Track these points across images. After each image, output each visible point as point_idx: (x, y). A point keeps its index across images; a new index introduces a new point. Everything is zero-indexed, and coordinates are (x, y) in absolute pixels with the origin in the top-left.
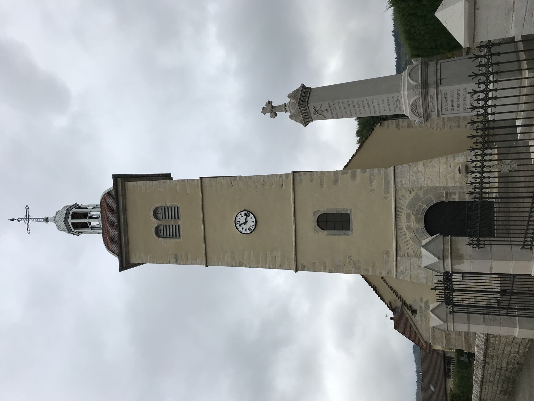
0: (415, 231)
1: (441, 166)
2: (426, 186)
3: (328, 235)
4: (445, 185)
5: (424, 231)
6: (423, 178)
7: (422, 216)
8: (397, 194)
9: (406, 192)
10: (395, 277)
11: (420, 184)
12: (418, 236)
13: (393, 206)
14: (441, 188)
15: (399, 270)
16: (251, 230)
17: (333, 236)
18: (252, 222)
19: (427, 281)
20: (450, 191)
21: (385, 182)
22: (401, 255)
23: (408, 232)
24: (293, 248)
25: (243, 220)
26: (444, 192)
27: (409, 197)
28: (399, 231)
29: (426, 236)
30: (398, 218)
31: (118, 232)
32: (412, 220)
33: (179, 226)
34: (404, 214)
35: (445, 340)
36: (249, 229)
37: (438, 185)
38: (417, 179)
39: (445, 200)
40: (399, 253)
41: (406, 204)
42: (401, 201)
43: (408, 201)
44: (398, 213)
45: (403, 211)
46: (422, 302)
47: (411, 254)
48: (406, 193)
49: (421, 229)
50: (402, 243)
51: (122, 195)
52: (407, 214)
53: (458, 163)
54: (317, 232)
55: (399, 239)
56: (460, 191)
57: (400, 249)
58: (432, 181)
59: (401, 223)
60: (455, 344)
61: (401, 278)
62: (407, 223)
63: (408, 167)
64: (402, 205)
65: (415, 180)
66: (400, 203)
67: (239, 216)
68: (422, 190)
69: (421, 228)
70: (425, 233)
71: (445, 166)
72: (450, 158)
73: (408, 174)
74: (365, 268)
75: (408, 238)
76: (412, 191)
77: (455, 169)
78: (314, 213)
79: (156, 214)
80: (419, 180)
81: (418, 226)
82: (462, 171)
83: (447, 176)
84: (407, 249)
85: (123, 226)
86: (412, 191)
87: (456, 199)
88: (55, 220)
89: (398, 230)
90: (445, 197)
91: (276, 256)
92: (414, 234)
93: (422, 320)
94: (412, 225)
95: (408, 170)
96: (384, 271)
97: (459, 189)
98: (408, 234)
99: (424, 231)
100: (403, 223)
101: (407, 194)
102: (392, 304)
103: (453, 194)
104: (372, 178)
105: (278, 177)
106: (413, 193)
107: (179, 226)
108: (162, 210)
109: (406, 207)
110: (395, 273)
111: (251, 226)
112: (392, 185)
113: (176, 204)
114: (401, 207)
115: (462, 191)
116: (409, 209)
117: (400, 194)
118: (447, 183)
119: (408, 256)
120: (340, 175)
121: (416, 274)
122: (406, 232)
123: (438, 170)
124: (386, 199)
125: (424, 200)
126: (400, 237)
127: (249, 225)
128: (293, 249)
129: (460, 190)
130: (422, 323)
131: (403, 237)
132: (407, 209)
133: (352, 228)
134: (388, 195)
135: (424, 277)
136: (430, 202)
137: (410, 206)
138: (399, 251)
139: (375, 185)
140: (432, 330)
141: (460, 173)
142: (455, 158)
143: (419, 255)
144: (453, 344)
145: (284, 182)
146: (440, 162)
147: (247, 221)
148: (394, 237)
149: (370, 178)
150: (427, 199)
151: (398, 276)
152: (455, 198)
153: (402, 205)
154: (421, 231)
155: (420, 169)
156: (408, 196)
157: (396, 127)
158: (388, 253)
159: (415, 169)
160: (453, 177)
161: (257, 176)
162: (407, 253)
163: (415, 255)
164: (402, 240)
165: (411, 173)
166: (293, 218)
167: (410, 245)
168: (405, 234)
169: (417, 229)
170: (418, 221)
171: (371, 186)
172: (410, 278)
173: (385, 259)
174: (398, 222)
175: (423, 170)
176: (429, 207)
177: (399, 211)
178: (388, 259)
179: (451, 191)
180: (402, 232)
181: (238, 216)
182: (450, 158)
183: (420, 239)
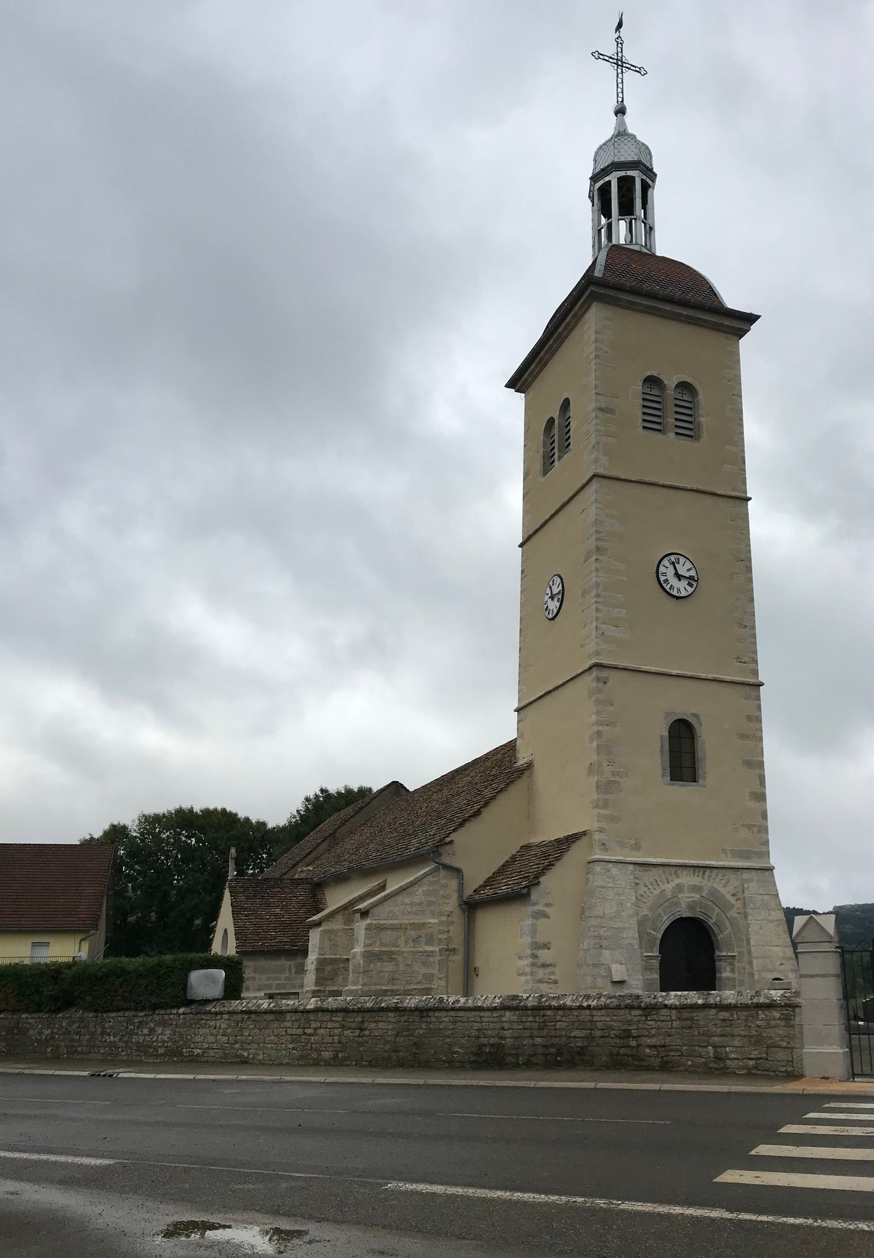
1: (780, 949)
2: (749, 922)
3: (662, 736)
6: (760, 918)
8: (730, 871)
11: (751, 911)
12: (667, 904)
13: (713, 863)
15: (610, 865)
16: (664, 585)
17: (660, 746)
18: (679, 590)
21: (749, 851)
24: (638, 666)
25: (682, 571)
26: (734, 952)
27: (726, 892)
28: (673, 870)
29: (667, 919)
30: (694, 871)
31: (693, 303)
32: (693, 895)
33: (660, 431)
34: (701, 882)
35: (380, 951)
36: (666, 581)
38: (758, 908)
40: (638, 868)
41: (716, 886)
46: (544, 906)
49: (678, 910)
50: (654, 876)
51: (722, 325)
52: (702, 886)
53: (787, 977)
54: (666, 718)
55: (660, 870)
57: (645, 871)
60: (372, 971)
62: (687, 886)
66: (717, 875)
67: (688, 565)
69: (680, 911)
70: (672, 917)
71: (781, 955)
74: (610, 802)
75: (663, 887)
76: (735, 898)
78: (696, 716)
79: (684, 386)
83: (766, 957)
85: (669, 309)
88: (621, 134)
89: (676, 868)
90: (729, 954)
91: (618, 627)
92: (669, 897)
93: (412, 904)
94: (683, 895)
98: (670, 886)
100: (688, 879)
101: (731, 888)
102: (447, 847)
104: (755, 830)
105: (752, 656)
107: (660, 431)
108: (657, 396)
111: (672, 586)
113: (705, 435)
114: (711, 876)
115: (737, 984)
117: (731, 876)
118: (756, 958)
120: (758, 771)
124: (724, 851)
126: (664, 872)
127: (673, 581)
128: (634, 666)
129: (739, 980)
130: (407, 904)
131: (664, 877)
133: (673, 785)
134: (730, 855)
135: (606, 912)
137: (713, 892)
140: (396, 924)
141: (774, 979)
144: (372, 967)
145: (745, 665)
147: (680, 580)
149: (755, 826)
152: (726, 971)
156: (728, 890)
158: (637, 847)
161: (753, 614)
162: (638, 884)
164: (660, 876)
165: (766, 898)
166: (689, 674)
167: (652, 890)
169: (677, 904)
170: (691, 906)
171: (743, 825)
172: (600, 885)
176: (712, 926)
177: (704, 873)
179: (737, 964)
181: (688, 562)
183: (662, 907)
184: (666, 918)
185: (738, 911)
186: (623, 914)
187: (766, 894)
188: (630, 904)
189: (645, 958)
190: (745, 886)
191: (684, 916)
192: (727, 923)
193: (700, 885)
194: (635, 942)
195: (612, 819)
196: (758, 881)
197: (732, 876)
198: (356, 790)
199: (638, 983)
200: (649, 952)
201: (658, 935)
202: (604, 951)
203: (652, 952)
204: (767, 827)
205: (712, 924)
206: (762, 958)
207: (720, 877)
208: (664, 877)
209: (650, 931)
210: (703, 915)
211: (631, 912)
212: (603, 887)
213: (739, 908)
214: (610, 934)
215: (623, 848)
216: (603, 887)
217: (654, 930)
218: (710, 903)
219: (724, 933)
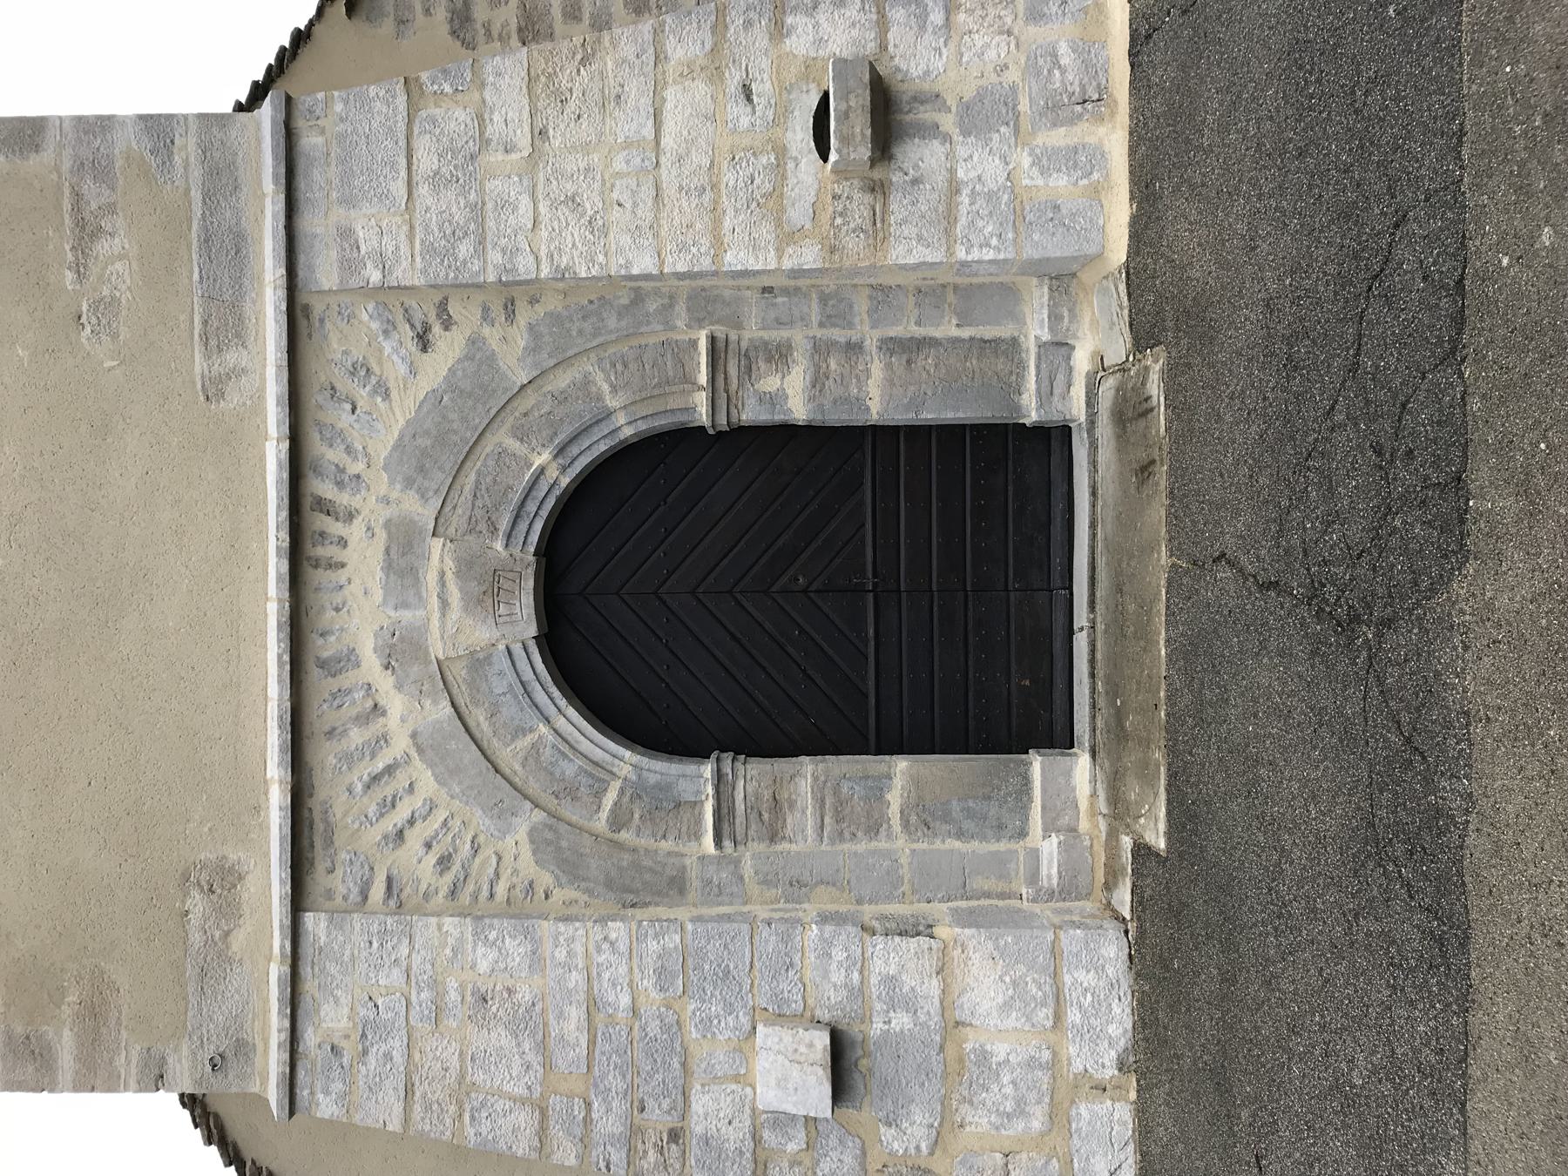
0: (458, 672)
1: (671, 94)
4: (706, 264)
5: (528, 675)
6: (525, 202)
7: (516, 551)
8: (307, 349)
9: (386, 332)
10: (274, 1095)
12: (479, 718)
13: (274, 454)
14: (671, 306)
15: (310, 1038)
19: (542, 1132)
20: (746, 335)
22: (339, 900)
23: (399, 687)
26: (694, 344)
28: (319, 685)
32: (432, 578)
37: (644, 264)
39: (702, 416)
40: (320, 880)
41: (383, 444)
42: (344, 419)
43: (399, 413)
44: (319, 522)
45: (356, 502)
47: (423, 887)
48: (388, 347)
49: (506, 663)
52: (388, 524)
53: (810, 67)
55: (324, 757)
56: (819, 333)
57: (329, 842)
58: (597, 228)
59: (337, 610)
61: (326, 1107)
63: (401, 100)
64: (349, 450)
65: (459, 217)
68: (524, 315)
71: (700, 89)
72: (748, 24)
73: (403, 162)
74: (19, 1029)
75: (400, 744)
76: (437, 329)
77: (782, 114)
80: (490, 223)
81: (482, 634)
82: (844, 116)
83: (714, 186)
84: (385, 837)
86: (437, 329)
87: (791, 403)
90: (703, 378)
95: (401, 126)
96: (185, 1051)
97: (815, 319)
99: (528, 675)
101: (394, 355)
103: (769, 360)
106: (449, 348)
109: (385, 468)
110: (274, 1061)
112: (269, 262)
115: (838, 335)
116: (409, 483)
118: (718, 245)
119: (392, 903)
121: (455, 1062)
122: (384, 683)
123: (648, 131)
124: (214, 389)
125: (538, 405)
129: (821, 325)
131: (357, 737)
132: (392, 482)
134: (232, 357)
135: (521, 1091)
136: (586, 430)
138: (321, 866)
139: (118, 266)
142: (789, 20)
143: (485, 893)
146: (659, 58)
148: (274, 739)
149: (77, 196)
150: (561, 398)
151: (303, 1094)
153: (349, 450)
154: (511, 676)
155: (495, 129)
156: (403, 369)
157: (453, 33)
159: (457, 119)
160: (768, 187)
162: (389, 880)
163: (453, 893)
164: (349, 759)
165: (426, 161)
168: (369, 704)
169: (478, 662)
171: (80, 277)
172: (398, 1108)
173: (196, 938)
174: (310, 597)
175: (527, 129)
178: (227, 934)
179: (752, 331)
180: (349, 692)
182: (748, 24)
184: (543, 729)
185: (497, 311)
186: (524, 994)
187: (409, 157)
188: (481, 950)
189: (727, 844)
190: (375, 277)
191: (532, 630)
192: (562, 380)
193: (381, 535)
194: (653, 946)
195: (94, 1015)
196: (349, 202)
197: (335, 347)
198: (233, 1167)
199: (839, 955)
200: (699, 820)
201: (625, 770)
202: (697, 1127)
203: (697, 805)
204: (79, 119)
205: (564, 469)
206: (715, 210)
207: (343, 418)
208: (357, 737)
209: (604, 814)
210: (523, 526)
211: (516, 949)
212: (409, 1090)
213: (486, 310)
214: (615, 1082)
215: (230, 961)
216: (409, 1090)
217: (599, 795)
218: (469, 480)
219: (612, 402)
